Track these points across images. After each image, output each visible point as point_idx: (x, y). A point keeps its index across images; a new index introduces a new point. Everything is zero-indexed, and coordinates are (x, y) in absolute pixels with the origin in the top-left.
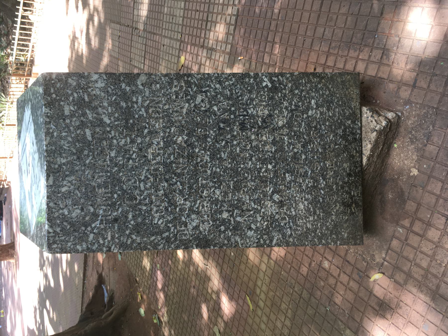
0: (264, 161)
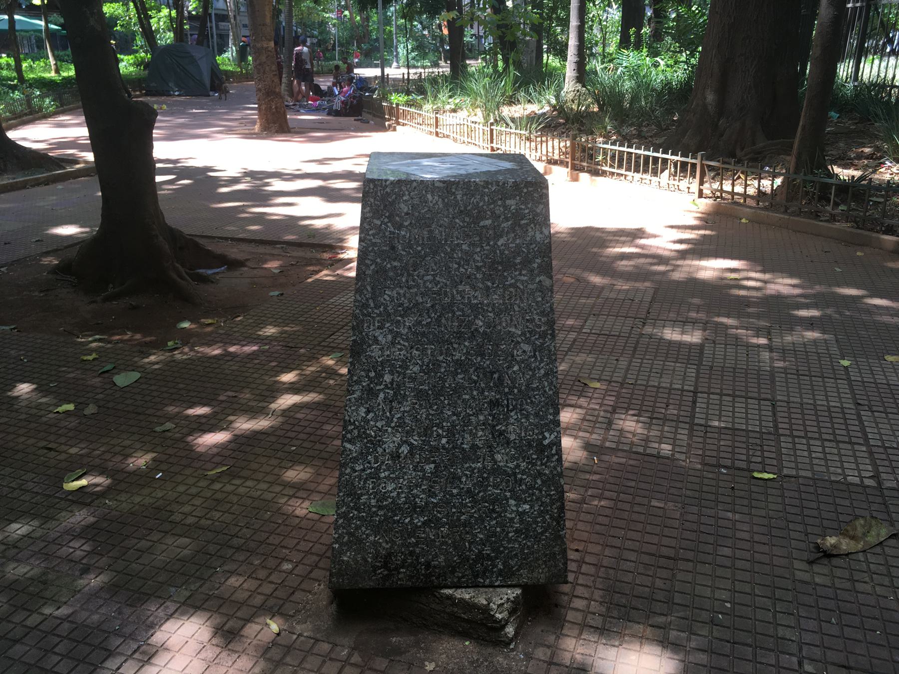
0: (451, 433)
